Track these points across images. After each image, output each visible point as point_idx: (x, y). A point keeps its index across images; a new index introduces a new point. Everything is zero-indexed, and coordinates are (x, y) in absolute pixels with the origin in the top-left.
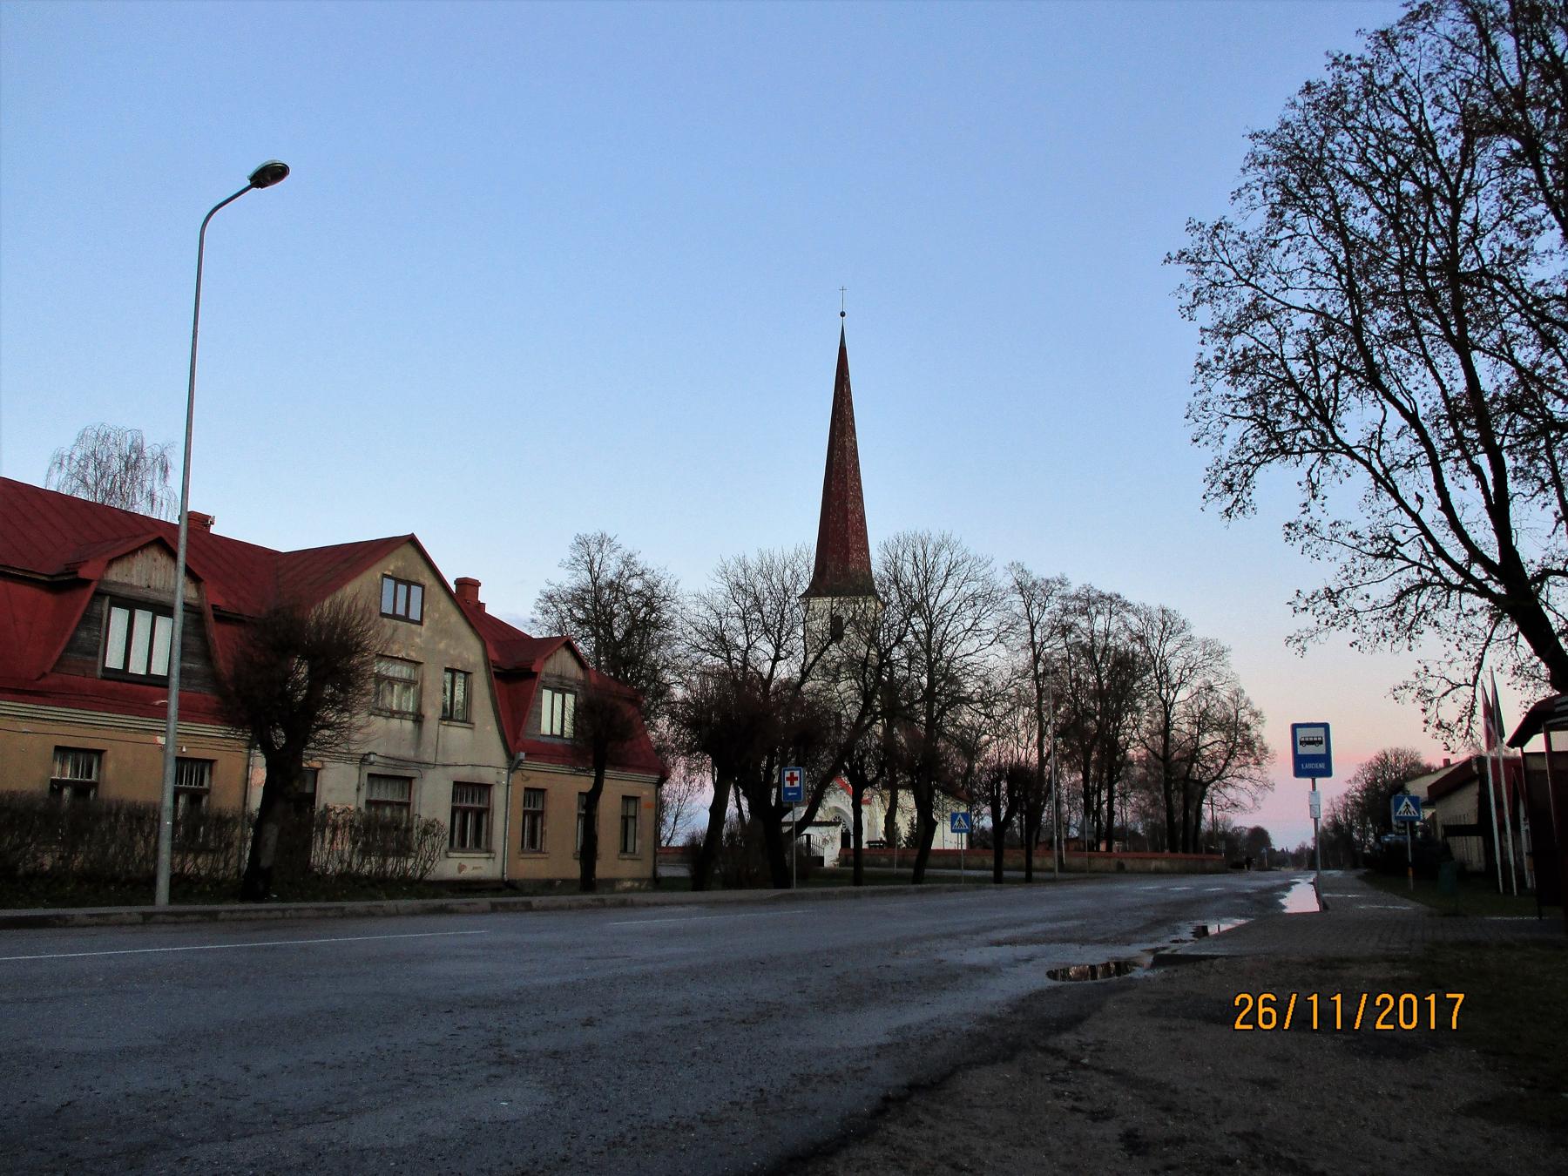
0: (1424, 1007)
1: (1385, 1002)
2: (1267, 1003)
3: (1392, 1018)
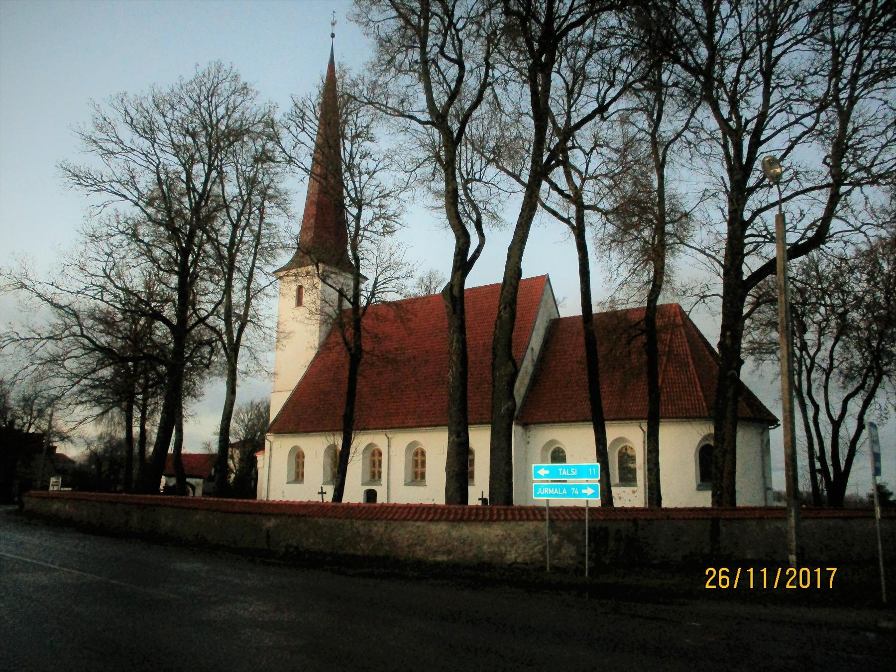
0: (814, 576)
1: (791, 573)
2: (724, 573)
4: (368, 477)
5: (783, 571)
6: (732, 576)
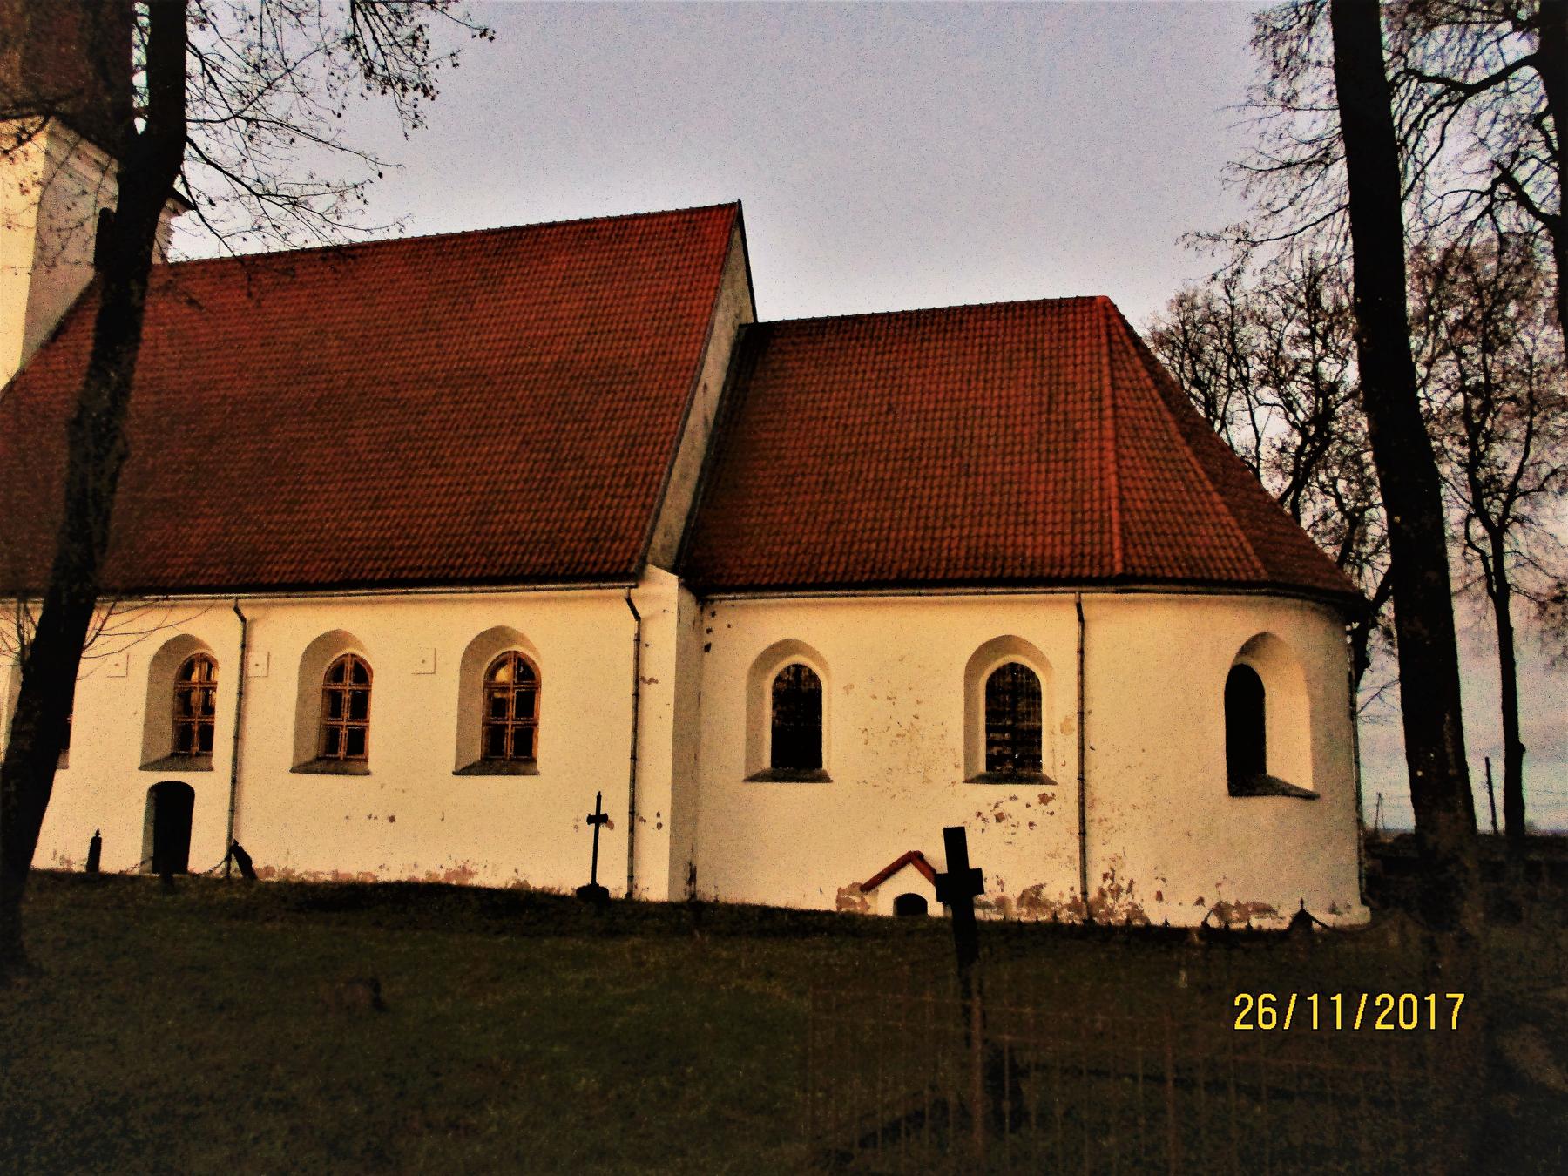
0: (1424, 1006)
1: (1385, 1002)
2: (1267, 1003)
3: (1392, 1018)
4: (165, 747)
5: (1371, 999)
6: (1281, 1008)
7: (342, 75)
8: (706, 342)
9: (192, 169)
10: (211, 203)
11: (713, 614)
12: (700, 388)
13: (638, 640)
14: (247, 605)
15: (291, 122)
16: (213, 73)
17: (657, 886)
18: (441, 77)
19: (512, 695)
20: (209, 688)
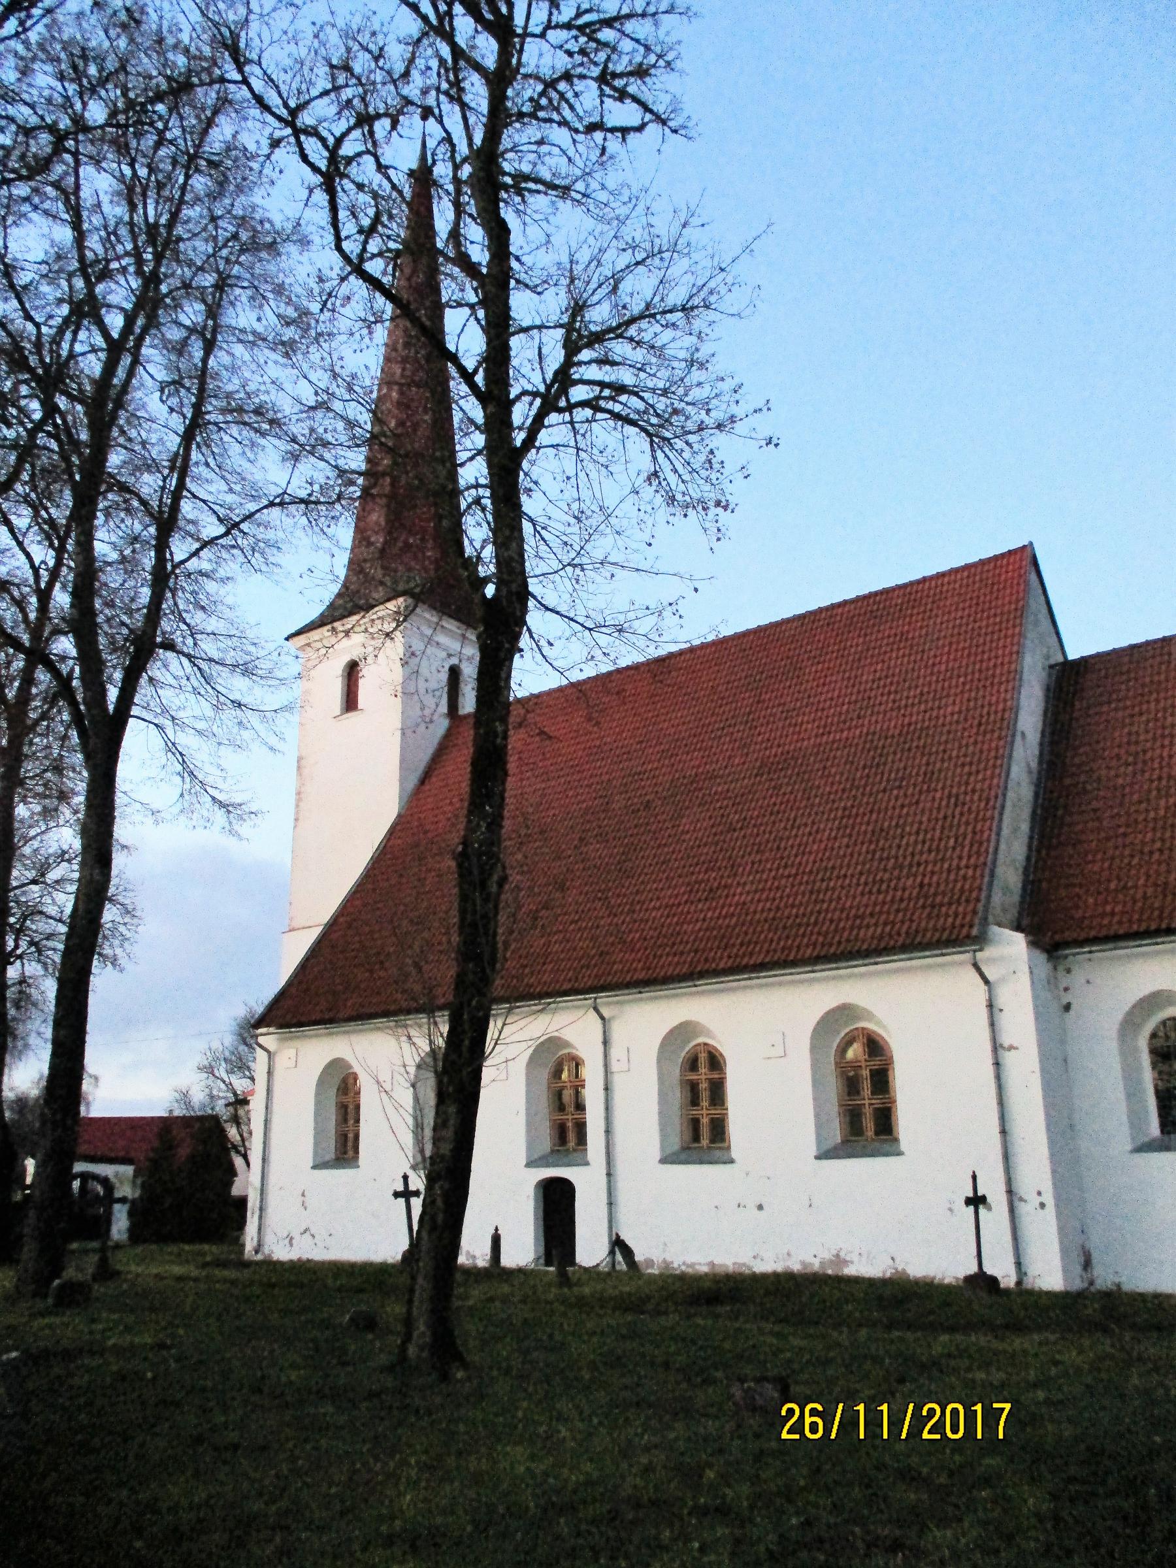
0: (971, 1417)
1: (932, 1412)
2: (814, 1412)
3: (938, 1428)
4: (546, 1144)
7: (649, 510)
8: (1017, 690)
9: (534, 617)
10: (551, 644)
11: (1069, 971)
12: (1018, 738)
13: (990, 1006)
14: (609, 1004)
15: (611, 559)
16: (543, 532)
17: (1050, 1274)
18: (736, 491)
19: (865, 1073)
20: (578, 1086)
